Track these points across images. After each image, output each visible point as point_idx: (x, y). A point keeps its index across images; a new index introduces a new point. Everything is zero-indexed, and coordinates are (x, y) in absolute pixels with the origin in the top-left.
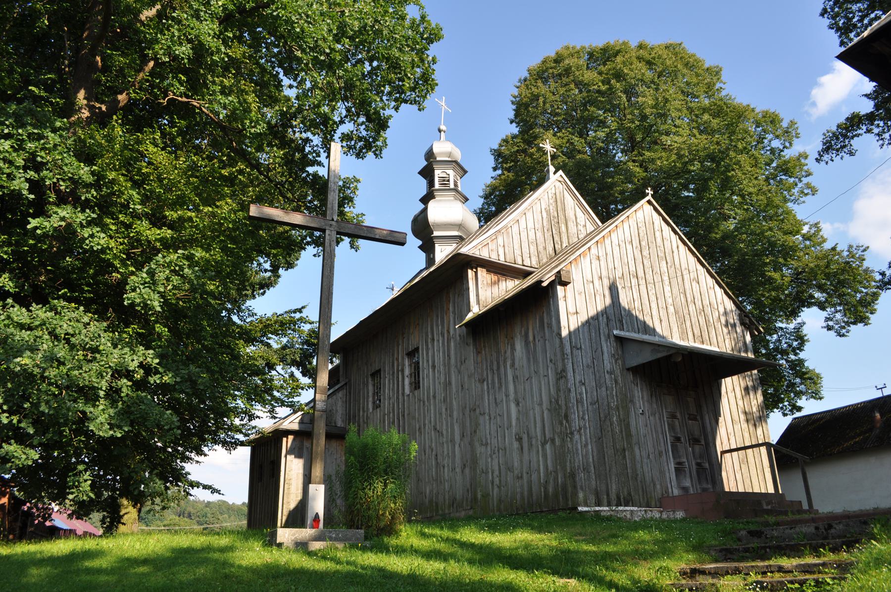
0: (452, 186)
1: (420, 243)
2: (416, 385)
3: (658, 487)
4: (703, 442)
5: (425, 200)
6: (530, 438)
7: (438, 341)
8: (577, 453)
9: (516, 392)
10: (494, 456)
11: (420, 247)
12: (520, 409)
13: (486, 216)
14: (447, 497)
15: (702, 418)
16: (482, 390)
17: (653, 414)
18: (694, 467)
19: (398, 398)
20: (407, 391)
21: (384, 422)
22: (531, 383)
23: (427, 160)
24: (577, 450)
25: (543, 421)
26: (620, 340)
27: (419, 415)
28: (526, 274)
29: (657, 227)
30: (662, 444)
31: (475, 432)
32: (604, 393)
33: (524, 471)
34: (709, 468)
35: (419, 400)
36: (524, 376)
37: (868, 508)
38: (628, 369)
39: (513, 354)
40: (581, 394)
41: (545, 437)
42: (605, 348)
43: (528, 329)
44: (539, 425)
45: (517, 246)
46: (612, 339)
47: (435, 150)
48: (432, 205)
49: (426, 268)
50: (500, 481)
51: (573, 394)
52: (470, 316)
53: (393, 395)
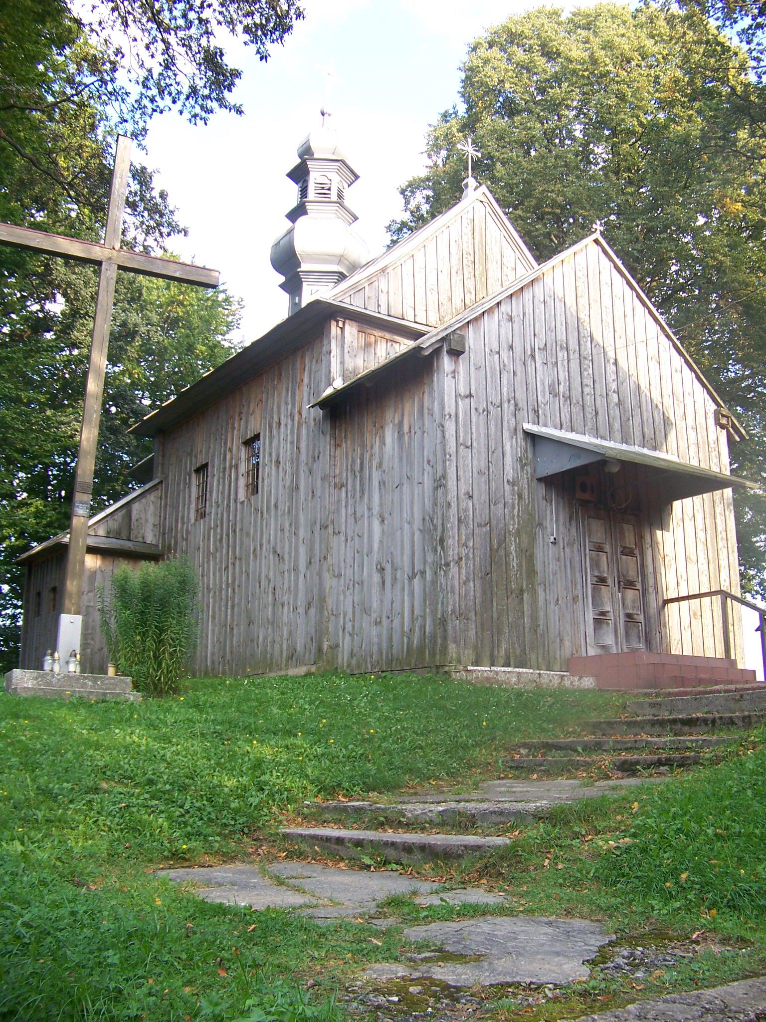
0: (334, 197)
1: (282, 279)
2: (254, 488)
3: (567, 644)
4: (639, 586)
5: (297, 213)
6: (395, 569)
7: (286, 425)
8: (453, 592)
9: (381, 505)
10: (348, 593)
11: (282, 286)
12: (385, 527)
14: (285, 646)
15: (642, 554)
16: (339, 501)
17: (571, 544)
18: (622, 619)
19: (228, 506)
20: (242, 496)
21: (209, 539)
22: (401, 492)
23: (300, 156)
24: (452, 588)
25: (413, 546)
26: (532, 438)
27: (255, 531)
28: (416, 335)
29: (605, 277)
30: (579, 587)
31: (325, 558)
32: (501, 511)
33: (385, 614)
34: (645, 625)
35: (256, 510)
36: (393, 483)
38: (540, 480)
39: (381, 449)
40: (466, 510)
41: (413, 568)
42: (508, 448)
43: (403, 415)
44: (407, 551)
45: (409, 293)
46: (520, 435)
50: (353, 627)
51: (453, 511)
52: (329, 391)
53: (223, 502)
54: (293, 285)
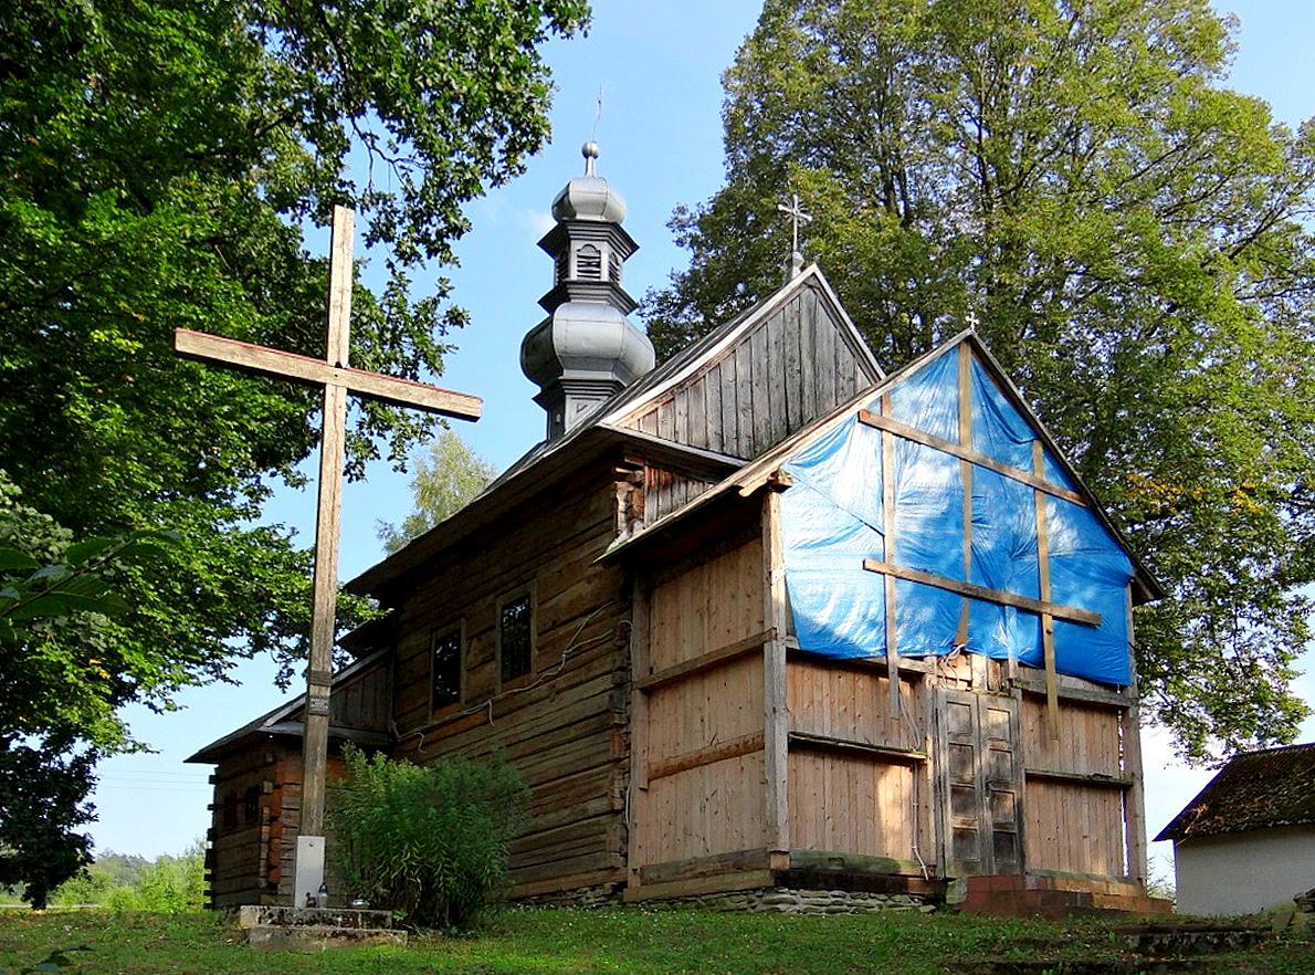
0: (605, 277)
1: (537, 390)
11: (537, 399)
13: (668, 340)
37: (863, 766)
47: (573, 197)
48: (562, 312)
49: (547, 442)
52: (615, 545)
54: (551, 399)
